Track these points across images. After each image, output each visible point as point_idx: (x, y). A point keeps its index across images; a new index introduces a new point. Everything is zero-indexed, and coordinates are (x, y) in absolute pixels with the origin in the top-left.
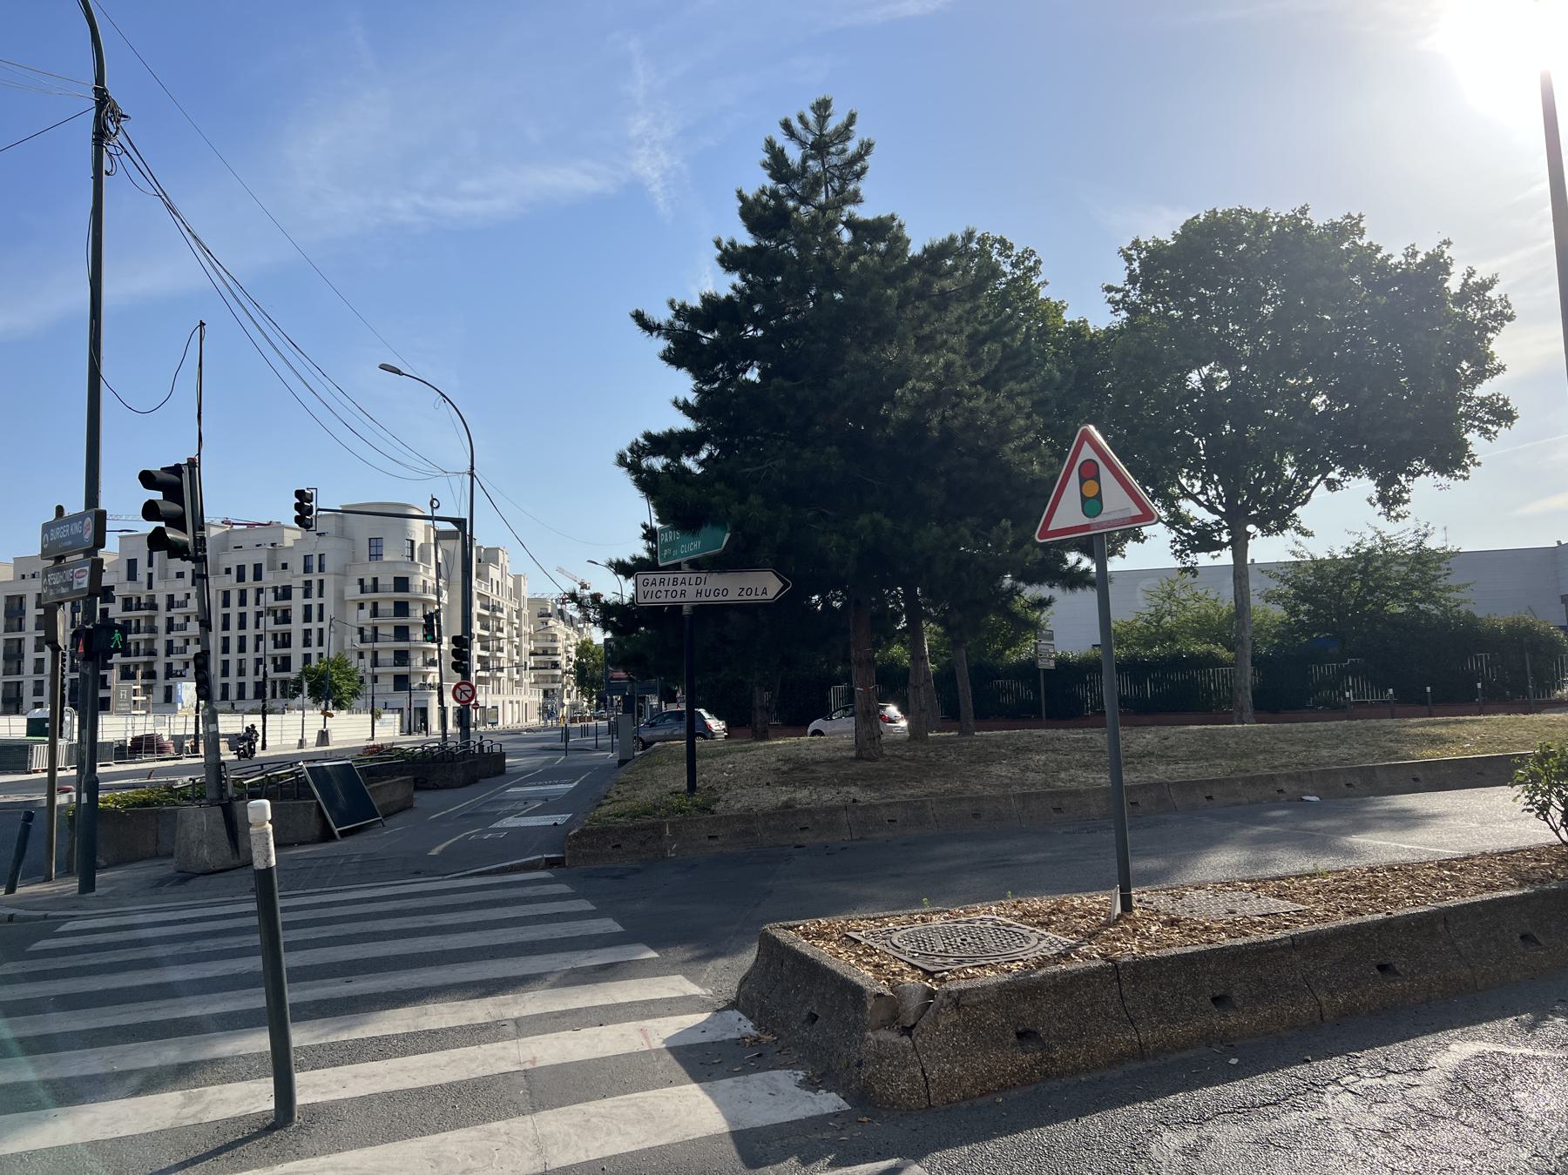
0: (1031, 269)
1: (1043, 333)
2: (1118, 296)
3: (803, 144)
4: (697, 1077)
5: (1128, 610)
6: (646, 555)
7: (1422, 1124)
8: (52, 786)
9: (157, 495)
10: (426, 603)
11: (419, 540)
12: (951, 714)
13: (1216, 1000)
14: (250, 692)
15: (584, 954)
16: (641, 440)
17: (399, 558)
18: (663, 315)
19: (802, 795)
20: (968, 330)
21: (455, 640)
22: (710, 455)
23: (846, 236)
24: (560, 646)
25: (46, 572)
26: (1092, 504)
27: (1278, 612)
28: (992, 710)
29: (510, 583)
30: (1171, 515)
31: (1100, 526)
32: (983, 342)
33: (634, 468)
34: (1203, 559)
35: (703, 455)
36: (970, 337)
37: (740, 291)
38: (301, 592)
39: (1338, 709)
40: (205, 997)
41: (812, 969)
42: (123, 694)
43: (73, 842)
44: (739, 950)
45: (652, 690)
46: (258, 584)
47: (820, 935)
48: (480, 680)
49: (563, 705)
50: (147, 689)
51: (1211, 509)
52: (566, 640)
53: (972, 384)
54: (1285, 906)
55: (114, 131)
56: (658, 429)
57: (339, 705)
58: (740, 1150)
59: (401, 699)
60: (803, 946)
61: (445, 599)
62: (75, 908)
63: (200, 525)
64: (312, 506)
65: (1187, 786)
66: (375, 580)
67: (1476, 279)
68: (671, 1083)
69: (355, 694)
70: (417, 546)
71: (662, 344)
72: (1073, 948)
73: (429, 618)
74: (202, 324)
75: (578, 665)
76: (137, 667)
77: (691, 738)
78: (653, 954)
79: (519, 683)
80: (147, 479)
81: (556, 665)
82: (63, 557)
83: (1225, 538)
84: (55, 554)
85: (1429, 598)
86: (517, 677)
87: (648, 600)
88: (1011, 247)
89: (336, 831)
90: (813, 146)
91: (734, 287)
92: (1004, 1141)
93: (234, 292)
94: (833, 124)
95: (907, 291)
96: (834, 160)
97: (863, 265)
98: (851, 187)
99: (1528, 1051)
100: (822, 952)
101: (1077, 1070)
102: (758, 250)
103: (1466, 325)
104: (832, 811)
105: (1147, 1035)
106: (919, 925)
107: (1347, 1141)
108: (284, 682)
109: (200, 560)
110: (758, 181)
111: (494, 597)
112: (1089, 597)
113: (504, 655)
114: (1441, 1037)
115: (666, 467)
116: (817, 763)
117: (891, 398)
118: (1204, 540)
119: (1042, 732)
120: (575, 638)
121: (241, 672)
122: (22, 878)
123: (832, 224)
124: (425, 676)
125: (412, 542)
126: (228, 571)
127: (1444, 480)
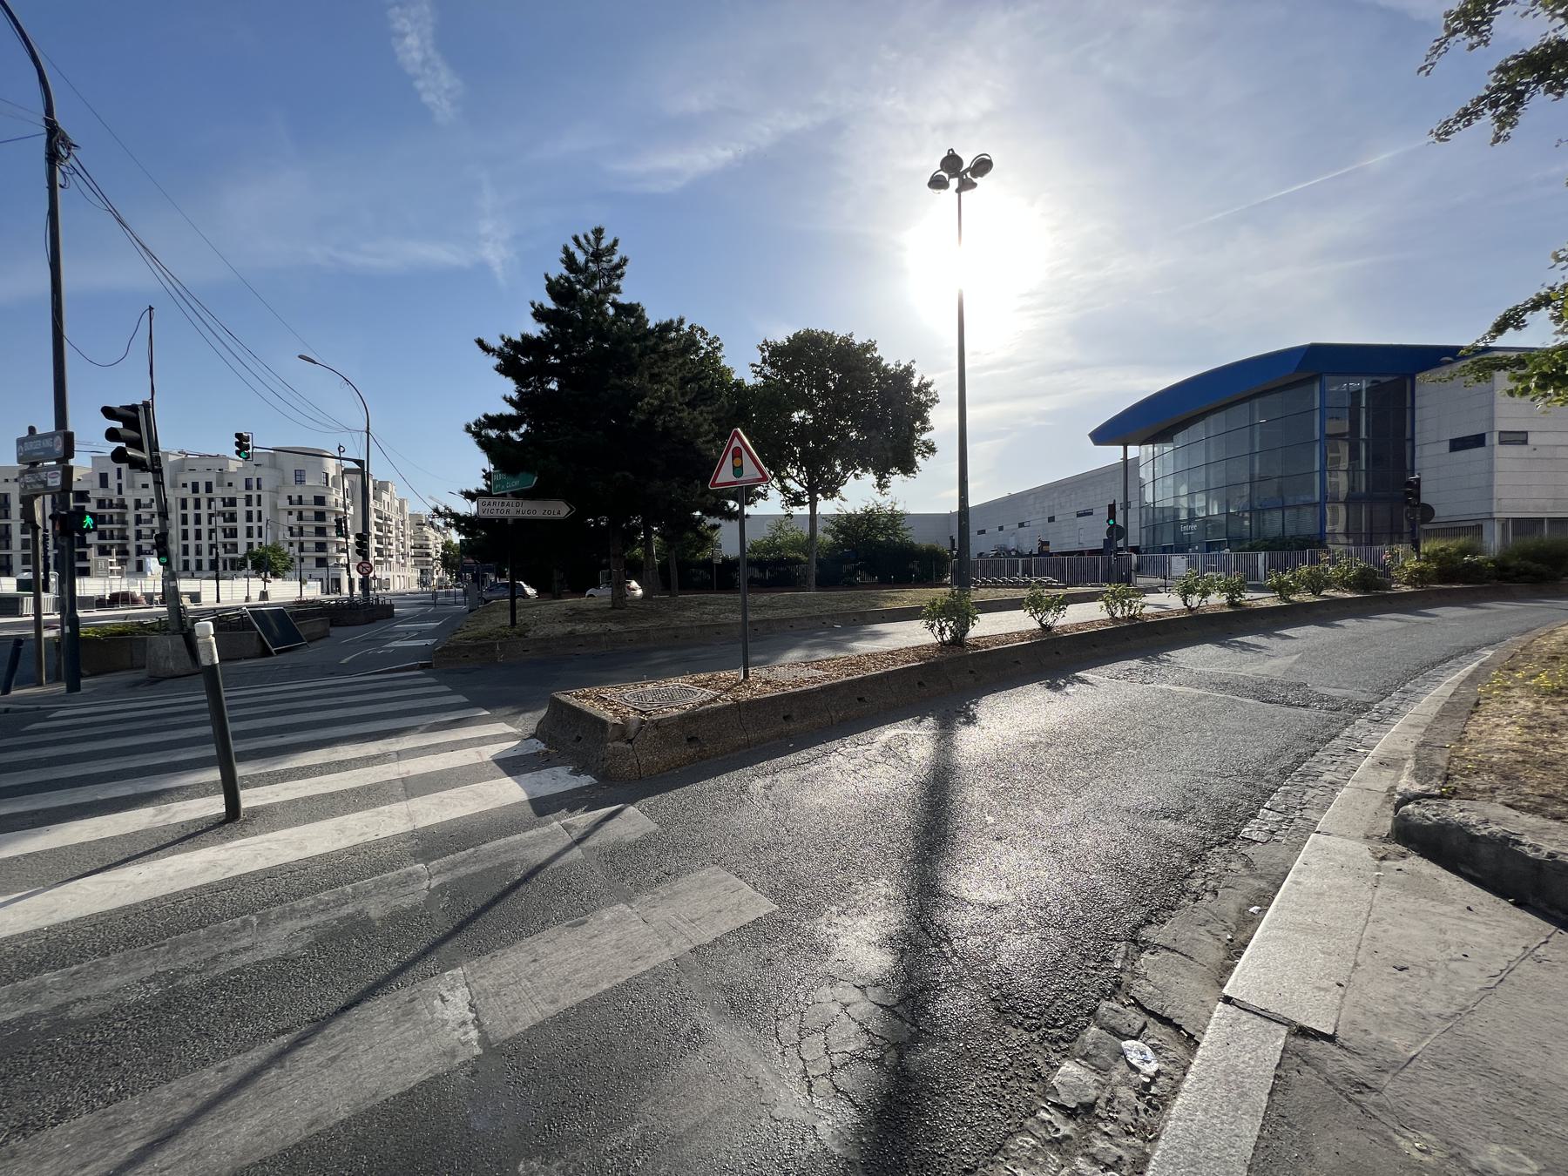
0: (717, 348)
1: (722, 384)
2: (758, 369)
3: (586, 252)
4: (510, 775)
5: (755, 535)
6: (485, 488)
7: (870, 766)
8: (38, 624)
9: (118, 425)
10: (337, 513)
11: (332, 473)
12: (666, 586)
13: (785, 718)
14: (206, 565)
15: (443, 715)
16: (483, 419)
17: (318, 484)
18: (497, 343)
19: (580, 627)
20: (680, 375)
21: (358, 536)
22: (527, 431)
23: (611, 311)
24: (431, 544)
25: (23, 473)
26: (738, 470)
27: (829, 538)
28: (687, 585)
29: (397, 503)
30: (782, 486)
31: (742, 482)
32: (688, 383)
33: (476, 435)
34: (796, 510)
35: (522, 430)
36: (681, 379)
37: (546, 335)
38: (244, 502)
39: (852, 585)
40: (173, 751)
41: (579, 714)
42: (101, 564)
43: (60, 659)
44: (541, 708)
45: (490, 570)
46: (210, 495)
47: (584, 697)
48: (377, 562)
49: (433, 579)
50: (121, 562)
51: (801, 484)
52: (435, 542)
53: (681, 404)
54: (819, 673)
55: (66, 155)
56: (493, 412)
57: (275, 575)
58: (534, 809)
59: (322, 572)
60: (574, 702)
61: (351, 511)
62: (64, 702)
63: (154, 446)
64: (248, 445)
65: (781, 621)
66: (300, 497)
67: (924, 381)
68: (494, 778)
69: (287, 568)
70: (330, 477)
71: (496, 361)
72: (719, 697)
73: (339, 521)
74: (151, 308)
75: (442, 555)
76: (112, 546)
77: (513, 598)
78: (487, 713)
79: (404, 565)
80: (108, 412)
81: (428, 555)
82: (37, 463)
83: (807, 500)
84: (30, 462)
85: (895, 534)
86: (403, 561)
87: (486, 514)
88: (707, 334)
89: (273, 650)
90: (592, 255)
91: (542, 332)
92: (677, 791)
93: (184, 296)
94: (604, 244)
95: (646, 347)
96: (605, 265)
97: (620, 328)
98: (615, 283)
99: (917, 732)
100: (586, 705)
101: (717, 755)
102: (557, 312)
103: (919, 403)
104: (597, 635)
105: (752, 736)
106: (640, 689)
107: (838, 777)
108: (233, 561)
109: (157, 470)
110: (558, 270)
111: (386, 512)
112: (735, 524)
113: (394, 547)
114: (882, 728)
115: (498, 437)
116: (589, 610)
117: (635, 407)
118: (796, 500)
119: (713, 595)
120: (441, 539)
121: (198, 552)
122: (16, 684)
123: (602, 303)
124: (338, 559)
125: (327, 474)
126: (185, 485)
127: (905, 478)
